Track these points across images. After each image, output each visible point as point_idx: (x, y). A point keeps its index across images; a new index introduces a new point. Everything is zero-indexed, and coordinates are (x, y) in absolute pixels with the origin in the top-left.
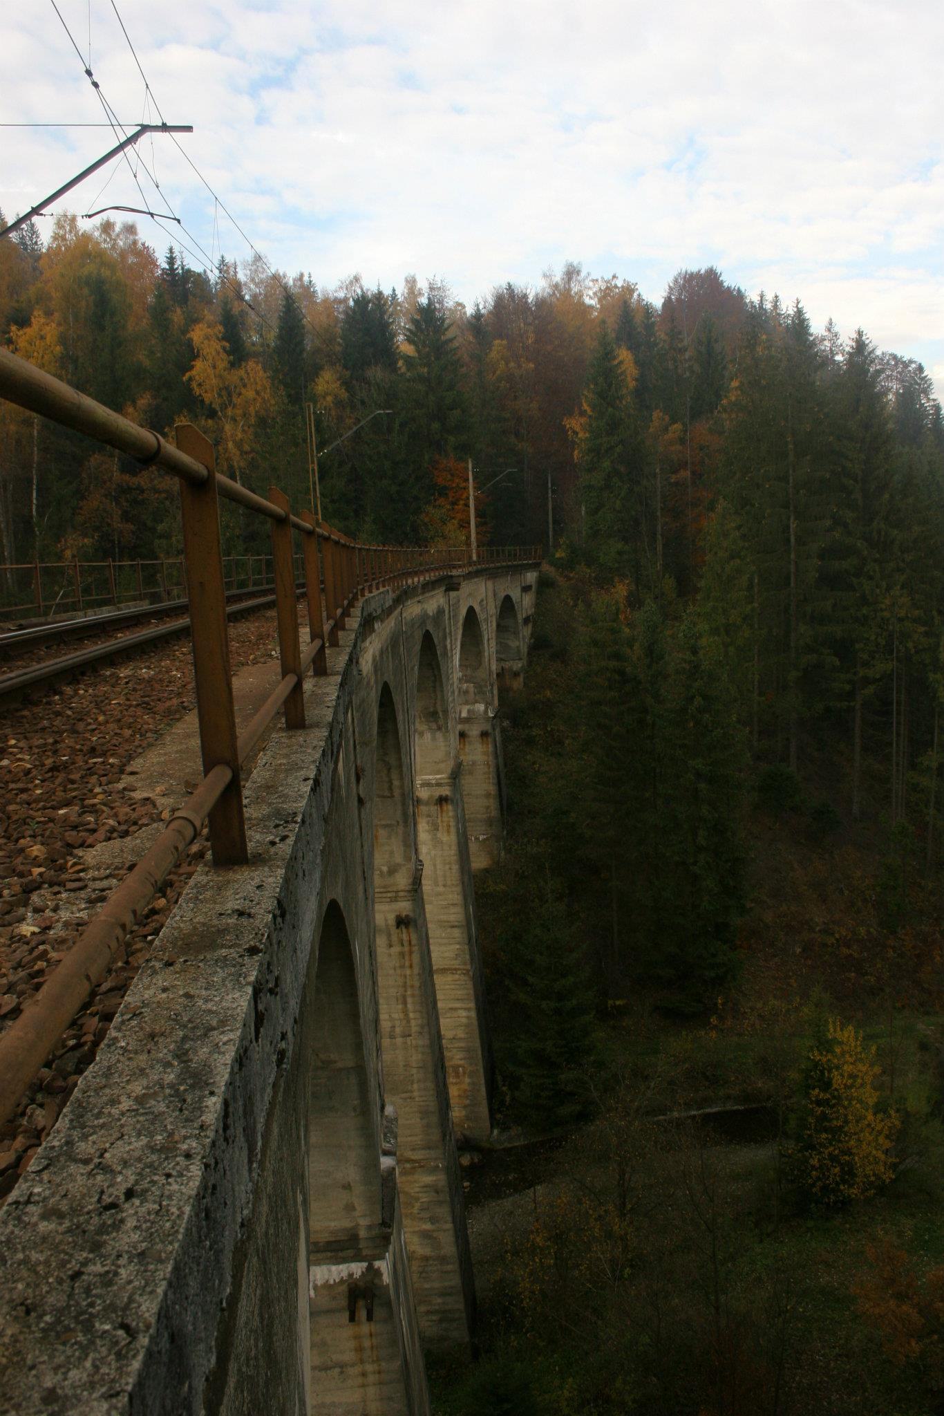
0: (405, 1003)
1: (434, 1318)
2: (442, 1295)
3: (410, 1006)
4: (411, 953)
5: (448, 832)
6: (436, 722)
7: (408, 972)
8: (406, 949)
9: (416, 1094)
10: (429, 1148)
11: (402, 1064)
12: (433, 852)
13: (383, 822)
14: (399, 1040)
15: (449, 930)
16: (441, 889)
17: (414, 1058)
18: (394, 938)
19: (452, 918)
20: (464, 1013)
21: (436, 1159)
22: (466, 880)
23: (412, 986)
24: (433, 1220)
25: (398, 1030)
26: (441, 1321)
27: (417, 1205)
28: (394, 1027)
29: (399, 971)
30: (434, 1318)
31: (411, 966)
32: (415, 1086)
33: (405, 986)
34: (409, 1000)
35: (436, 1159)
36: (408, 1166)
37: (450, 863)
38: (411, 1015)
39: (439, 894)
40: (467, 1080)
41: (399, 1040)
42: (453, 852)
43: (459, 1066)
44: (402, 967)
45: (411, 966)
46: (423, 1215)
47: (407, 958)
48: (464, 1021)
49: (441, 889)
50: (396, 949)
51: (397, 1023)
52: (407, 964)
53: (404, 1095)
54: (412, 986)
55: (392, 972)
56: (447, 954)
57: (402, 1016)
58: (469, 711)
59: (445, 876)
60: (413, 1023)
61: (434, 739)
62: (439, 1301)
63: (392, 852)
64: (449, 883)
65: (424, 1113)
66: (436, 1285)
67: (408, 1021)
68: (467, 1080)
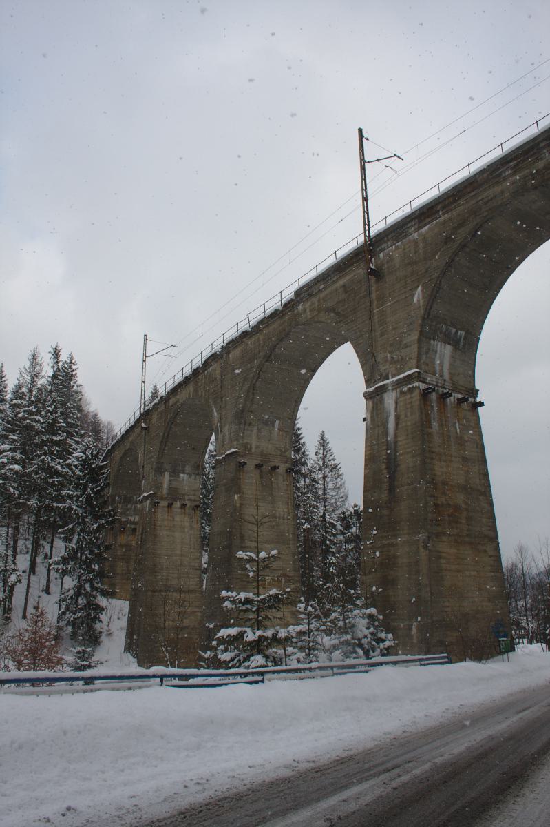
0: (288, 505)
18: (285, 478)
41: (286, 521)
61: (195, 479)
63: (286, 443)
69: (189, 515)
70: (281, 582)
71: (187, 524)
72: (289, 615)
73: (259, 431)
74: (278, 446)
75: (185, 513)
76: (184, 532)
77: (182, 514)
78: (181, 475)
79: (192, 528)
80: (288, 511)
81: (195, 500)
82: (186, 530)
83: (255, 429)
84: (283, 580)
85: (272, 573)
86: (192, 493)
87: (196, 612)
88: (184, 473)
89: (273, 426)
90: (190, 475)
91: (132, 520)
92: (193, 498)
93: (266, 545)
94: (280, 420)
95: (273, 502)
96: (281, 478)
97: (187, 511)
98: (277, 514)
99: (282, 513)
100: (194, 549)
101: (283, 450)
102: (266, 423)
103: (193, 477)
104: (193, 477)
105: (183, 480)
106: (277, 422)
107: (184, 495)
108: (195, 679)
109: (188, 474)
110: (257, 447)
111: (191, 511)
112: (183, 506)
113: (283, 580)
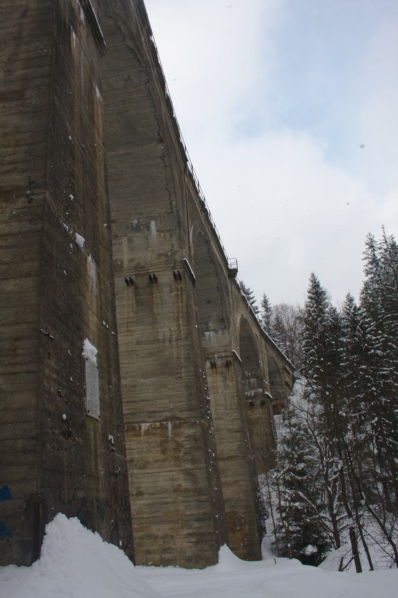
0: (178, 321)
1: (193, 540)
2: (198, 520)
3: (181, 323)
4: (182, 294)
5: (232, 380)
6: (224, 324)
7: (180, 304)
8: (180, 293)
9: (183, 375)
10: (191, 410)
11: (175, 356)
12: (224, 392)
13: (168, 229)
14: (174, 343)
15: (234, 434)
16: (229, 411)
17: (182, 353)
18: (173, 287)
19: (235, 427)
20: (244, 483)
21: (195, 417)
22: (215, 257)
23: (182, 312)
24: (193, 461)
25: (174, 337)
26: (197, 543)
27: (183, 450)
28: (171, 335)
29: (175, 305)
30: (193, 540)
31: (182, 301)
32: (183, 370)
33: (178, 312)
34: (181, 319)
35: (195, 417)
36: (177, 422)
37: (233, 397)
38: (182, 328)
39: (228, 414)
40: (247, 527)
41: (174, 343)
42: (234, 391)
43: (242, 518)
44: (177, 302)
45: (182, 301)
46: (188, 457)
47: (180, 297)
48: (245, 488)
49: (229, 411)
50: (174, 293)
51: (174, 333)
52: (180, 300)
53: (176, 376)
54: (182, 312)
55: (171, 305)
56: (233, 448)
57: (176, 328)
58: (255, 393)
59: (231, 404)
60: (182, 332)
61: (223, 334)
62: (197, 525)
63: (173, 245)
64: (233, 407)
65: (188, 387)
66: (195, 512)
67: (180, 332)
68: (247, 527)
69: (222, 373)
70: (167, 428)
71: (220, 384)
72: (181, 476)
73: (130, 241)
74: (161, 252)
75: (216, 373)
76: (217, 393)
77: (213, 374)
78: (206, 333)
79: (226, 386)
80: (179, 328)
81: (226, 357)
82: (220, 390)
83: (125, 239)
84: (170, 425)
85: (150, 417)
86: (224, 349)
87: (237, 481)
88: (208, 330)
89: (148, 228)
90: (216, 331)
91: (249, 395)
92: (223, 354)
93: (142, 380)
94: (155, 219)
95: (154, 322)
96: (166, 290)
97: (219, 369)
98: (161, 337)
99: (168, 334)
100: (231, 409)
101: (169, 254)
102: (137, 229)
103: (220, 332)
104: (220, 332)
105: (210, 338)
106: (153, 223)
107: (213, 353)
108: (364, 553)
109: (214, 330)
110: (131, 261)
111: (224, 369)
112: (213, 365)
113: (170, 425)
